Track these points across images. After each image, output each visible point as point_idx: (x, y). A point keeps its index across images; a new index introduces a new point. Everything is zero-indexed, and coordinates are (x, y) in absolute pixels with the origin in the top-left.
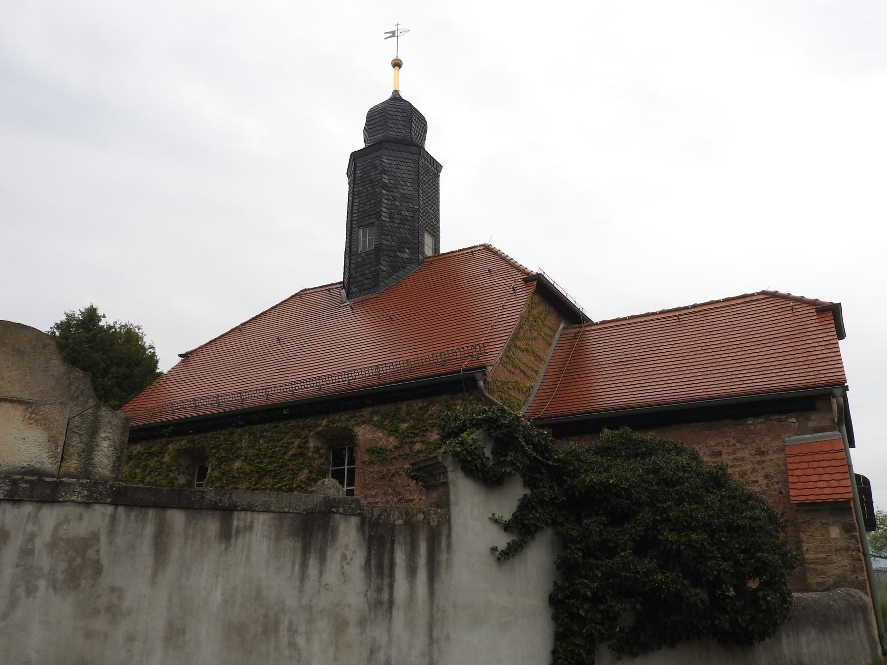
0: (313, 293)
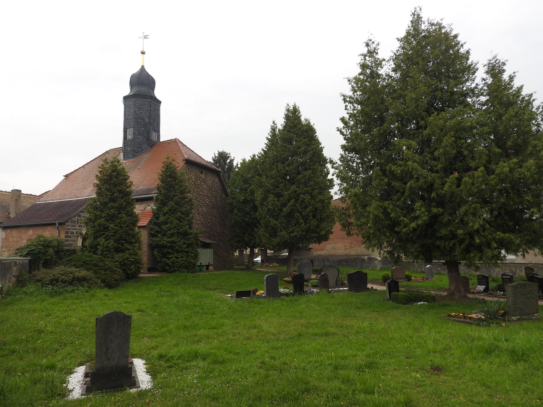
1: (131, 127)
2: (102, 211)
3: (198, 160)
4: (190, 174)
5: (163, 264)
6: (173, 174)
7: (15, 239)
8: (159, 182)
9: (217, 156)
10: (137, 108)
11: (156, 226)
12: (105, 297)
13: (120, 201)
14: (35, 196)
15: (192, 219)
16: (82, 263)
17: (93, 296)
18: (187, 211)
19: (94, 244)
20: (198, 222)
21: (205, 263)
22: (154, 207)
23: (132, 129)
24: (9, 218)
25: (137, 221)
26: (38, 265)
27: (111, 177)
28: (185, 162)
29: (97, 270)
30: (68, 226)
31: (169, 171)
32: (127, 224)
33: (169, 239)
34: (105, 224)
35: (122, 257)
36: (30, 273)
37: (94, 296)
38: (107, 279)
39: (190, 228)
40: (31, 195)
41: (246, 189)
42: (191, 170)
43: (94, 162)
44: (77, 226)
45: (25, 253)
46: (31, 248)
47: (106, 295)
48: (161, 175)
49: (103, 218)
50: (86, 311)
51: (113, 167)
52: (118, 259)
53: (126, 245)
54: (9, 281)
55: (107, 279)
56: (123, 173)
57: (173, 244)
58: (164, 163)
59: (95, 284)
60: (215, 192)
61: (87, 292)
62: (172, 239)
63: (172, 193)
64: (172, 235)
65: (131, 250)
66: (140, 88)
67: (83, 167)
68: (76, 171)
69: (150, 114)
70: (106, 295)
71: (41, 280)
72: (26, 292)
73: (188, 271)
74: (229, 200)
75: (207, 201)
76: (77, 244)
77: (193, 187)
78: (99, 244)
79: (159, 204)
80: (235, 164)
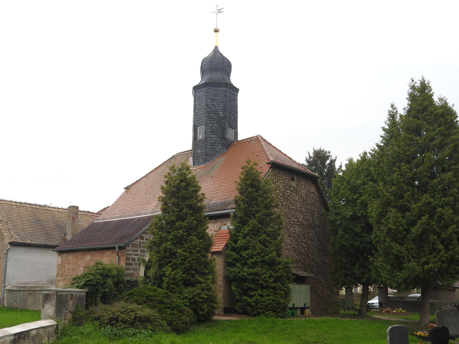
0: (178, 156)
2: (169, 233)
3: (288, 163)
4: (278, 182)
5: (243, 304)
6: (254, 182)
7: (71, 265)
8: (237, 193)
10: (210, 99)
13: (190, 219)
14: (93, 213)
15: (281, 242)
18: (274, 231)
19: (158, 274)
23: (204, 126)
24: (65, 240)
26: (96, 300)
27: (179, 189)
28: (270, 166)
29: (162, 308)
31: (249, 179)
32: (199, 249)
33: (251, 270)
34: (171, 249)
35: (192, 292)
36: (87, 309)
38: (174, 321)
39: (279, 255)
40: (89, 212)
41: (354, 201)
42: (278, 176)
44: (139, 250)
45: (82, 283)
46: (88, 278)
49: (169, 241)
52: (187, 295)
53: (197, 276)
54: (65, 317)
55: (174, 321)
56: (193, 182)
57: (256, 277)
58: (243, 168)
59: (160, 327)
60: (311, 205)
61: (151, 336)
62: (255, 270)
64: (255, 264)
68: (138, 181)
69: (226, 106)
71: (99, 319)
72: (83, 333)
75: (301, 218)
76: (139, 273)
78: (164, 275)
79: (238, 223)
80: (337, 166)
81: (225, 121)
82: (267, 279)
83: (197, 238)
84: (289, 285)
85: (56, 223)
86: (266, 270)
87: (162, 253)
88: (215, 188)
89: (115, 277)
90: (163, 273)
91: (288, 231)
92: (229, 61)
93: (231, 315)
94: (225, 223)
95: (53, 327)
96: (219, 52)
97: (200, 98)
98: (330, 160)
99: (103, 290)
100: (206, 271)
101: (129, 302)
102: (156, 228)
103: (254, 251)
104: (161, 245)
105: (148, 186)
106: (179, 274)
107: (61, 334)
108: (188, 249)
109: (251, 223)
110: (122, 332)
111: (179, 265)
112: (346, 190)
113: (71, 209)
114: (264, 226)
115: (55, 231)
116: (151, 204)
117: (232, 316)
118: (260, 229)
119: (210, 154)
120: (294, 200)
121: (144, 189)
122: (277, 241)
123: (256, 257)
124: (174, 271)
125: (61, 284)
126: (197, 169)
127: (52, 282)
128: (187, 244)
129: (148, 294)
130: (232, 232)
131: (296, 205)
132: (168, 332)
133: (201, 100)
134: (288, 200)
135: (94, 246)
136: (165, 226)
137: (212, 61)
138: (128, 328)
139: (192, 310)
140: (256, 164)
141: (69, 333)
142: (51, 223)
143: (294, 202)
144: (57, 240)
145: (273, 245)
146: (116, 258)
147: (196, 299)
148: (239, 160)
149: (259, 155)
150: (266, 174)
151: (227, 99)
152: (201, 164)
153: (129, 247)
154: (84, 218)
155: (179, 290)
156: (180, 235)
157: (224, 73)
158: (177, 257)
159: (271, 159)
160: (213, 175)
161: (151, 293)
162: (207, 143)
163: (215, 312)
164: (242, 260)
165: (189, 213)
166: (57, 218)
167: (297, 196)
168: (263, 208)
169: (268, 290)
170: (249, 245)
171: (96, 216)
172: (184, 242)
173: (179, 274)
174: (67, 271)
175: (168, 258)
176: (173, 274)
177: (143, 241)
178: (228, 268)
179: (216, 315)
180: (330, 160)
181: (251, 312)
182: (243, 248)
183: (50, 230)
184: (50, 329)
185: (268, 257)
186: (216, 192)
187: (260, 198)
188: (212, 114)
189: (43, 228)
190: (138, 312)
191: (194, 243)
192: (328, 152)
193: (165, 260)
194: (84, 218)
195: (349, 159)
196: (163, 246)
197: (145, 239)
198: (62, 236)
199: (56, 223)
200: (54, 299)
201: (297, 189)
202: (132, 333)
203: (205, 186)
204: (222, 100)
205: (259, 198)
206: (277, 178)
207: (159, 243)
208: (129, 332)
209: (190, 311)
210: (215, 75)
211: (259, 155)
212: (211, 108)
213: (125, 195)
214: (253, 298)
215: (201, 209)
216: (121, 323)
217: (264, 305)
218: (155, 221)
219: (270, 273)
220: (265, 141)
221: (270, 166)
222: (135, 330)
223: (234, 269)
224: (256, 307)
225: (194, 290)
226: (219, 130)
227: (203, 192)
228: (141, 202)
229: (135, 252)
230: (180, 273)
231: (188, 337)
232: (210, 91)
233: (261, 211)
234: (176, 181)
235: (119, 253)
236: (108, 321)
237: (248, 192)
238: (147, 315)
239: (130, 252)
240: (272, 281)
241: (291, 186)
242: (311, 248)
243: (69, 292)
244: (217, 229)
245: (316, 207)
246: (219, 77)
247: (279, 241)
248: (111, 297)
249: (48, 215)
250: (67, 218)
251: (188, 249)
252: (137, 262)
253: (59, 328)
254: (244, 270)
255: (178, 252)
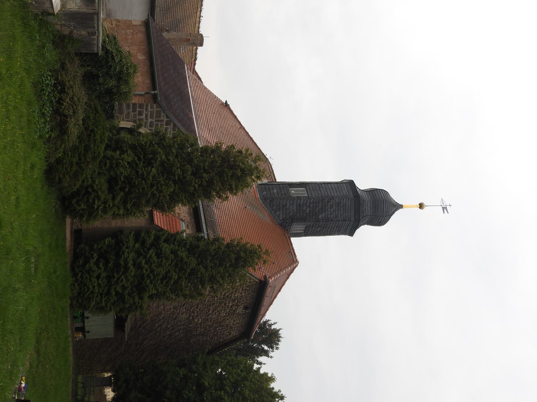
0: (268, 166)
1: (309, 193)
2: (177, 157)
3: (266, 300)
4: (243, 290)
5: (87, 254)
6: (242, 261)
7: (131, 37)
8: (227, 240)
9: (272, 328)
10: (339, 201)
11: (154, 239)
12: (29, 165)
13: (195, 182)
14: (195, 64)
15: (167, 298)
16: (90, 129)
17: (33, 146)
18: (181, 290)
19: (123, 145)
20: (162, 307)
21: (88, 325)
22: (185, 235)
23: (306, 195)
24: (162, 30)
25: (162, 210)
26: (88, 66)
27: (233, 167)
28: (263, 279)
29: (80, 151)
30: (152, 107)
31: (246, 255)
32: (158, 195)
33: (131, 262)
34: (156, 160)
35: (101, 189)
36: (77, 54)
37: (32, 148)
38: (63, 167)
39: (151, 297)
40: (196, 59)
41: (222, 388)
42: (249, 290)
43: (250, 142)
44: (152, 120)
45: (109, 48)
46: (116, 55)
47: (33, 167)
48: (238, 243)
49: (166, 157)
50: (5, 135)
51: (250, 170)
52: (97, 183)
53: (122, 194)
54: (64, 25)
55: (63, 167)
56: (241, 185)
57: (122, 269)
58: (259, 246)
59: (54, 149)
60: (214, 332)
61: (41, 137)
62: (132, 267)
63: (210, 262)
64: (138, 266)
65: (113, 203)
66: (369, 203)
67: (242, 128)
68: (235, 117)
69: (332, 221)
70: (34, 166)
71: (63, 68)
72: (44, 48)
73: (75, 297)
74: (202, 358)
75: (198, 320)
76: (123, 120)
77: (221, 296)
78: (123, 152)
79: (191, 243)
80: (262, 359)
81: (313, 221)
82: (120, 283)
83: (171, 192)
84: (113, 311)
85: (181, 19)
86: (132, 282)
87: (151, 149)
88: (232, 212)
89: (118, 90)
90: (125, 151)
91: (181, 305)
92: (386, 223)
93: (73, 240)
94: (189, 227)
95: (51, 9)
96: (396, 211)
97: (340, 189)
98: (268, 349)
99: (101, 75)
100: (129, 206)
101: (86, 107)
102: (182, 140)
103: (156, 265)
104: (161, 148)
105: (230, 130)
106: (124, 172)
107: (41, 19)
108: (156, 182)
109: (191, 260)
110: (46, 98)
111: (136, 170)
112: (235, 376)
113: (199, 37)
114: (187, 276)
115: (172, 18)
116: (209, 134)
117: (71, 241)
118: (184, 271)
119: (272, 205)
120: (220, 311)
121: (226, 125)
122: (169, 294)
123: (148, 268)
124: (127, 164)
125: (107, 25)
126: (253, 188)
127: (109, 15)
128: (163, 180)
129: (97, 132)
130: (178, 236)
131: (214, 313)
132: (48, 159)
133: (338, 191)
134: (219, 303)
135: (156, 65)
136: (185, 151)
137: (384, 202)
138: (51, 107)
139: (78, 189)
140: (265, 262)
141: (44, 29)
142: (182, 14)
143: (218, 311)
144: (161, 21)
145: (164, 289)
146: (142, 92)
147: (91, 194)
148: (267, 241)
149: (275, 265)
150: (253, 276)
151: (340, 222)
152: (260, 193)
153: (156, 108)
154: (188, 53)
155: (103, 172)
156: (174, 170)
157: (371, 217)
158: (146, 168)
159: (271, 280)
160: (248, 209)
161: (98, 136)
162: (286, 200)
163: (76, 219)
164: (144, 251)
165: (202, 181)
166: (188, 21)
167: (226, 314)
168: (211, 274)
169: (106, 286)
170: (164, 259)
171: (191, 68)
172: (165, 176)
173: (124, 172)
174: (123, 32)
175: (144, 157)
176: (123, 163)
177: (164, 125)
178: (133, 233)
179: (72, 220)
180: (268, 349)
181: (77, 264)
182: (159, 250)
183: (173, 12)
184: (47, 5)
185: (148, 284)
186: (227, 214)
187: (223, 269)
188: (321, 204)
189: (175, 3)
190: (73, 120)
191: (165, 189)
192: (278, 347)
193: (142, 153)
194: (188, 54)
195: (274, 377)
196: (160, 150)
197: (166, 127)
198: (166, 27)
199: (181, 19)
200: (88, 10)
201: (234, 314)
202: (45, 111)
203: (234, 200)
204: (339, 217)
205: (223, 268)
206: (248, 288)
207: (163, 144)
208: (47, 108)
209: (76, 187)
210: (369, 206)
211: (275, 265)
212: (329, 203)
213: (218, 102)
214: (95, 266)
215: (208, 196)
216: (59, 97)
217: (87, 281)
218: (190, 139)
219: (128, 287)
220: (292, 271)
221: (262, 280)
222: (49, 115)
223: (132, 240)
224: (84, 270)
225: (104, 191)
226: (302, 215)
227: (229, 198)
228: (211, 122)
229: (150, 115)
230: (126, 172)
231: (41, 185)
232: (349, 201)
233: (206, 271)
234: (243, 163)
235: (148, 95)
236: (60, 80)
237: (230, 253)
238: (70, 131)
239: (149, 110)
240: (117, 289)
241: (238, 307)
242: (160, 335)
243: (98, 30)
244: (182, 216)
245: (212, 338)
246: (367, 211)
247: (169, 297)
248: (92, 86)
249: (191, 10)
250: (188, 32)
251: (156, 182)
252: (137, 118)
253: (49, 17)
254: (131, 253)
255: (153, 169)
